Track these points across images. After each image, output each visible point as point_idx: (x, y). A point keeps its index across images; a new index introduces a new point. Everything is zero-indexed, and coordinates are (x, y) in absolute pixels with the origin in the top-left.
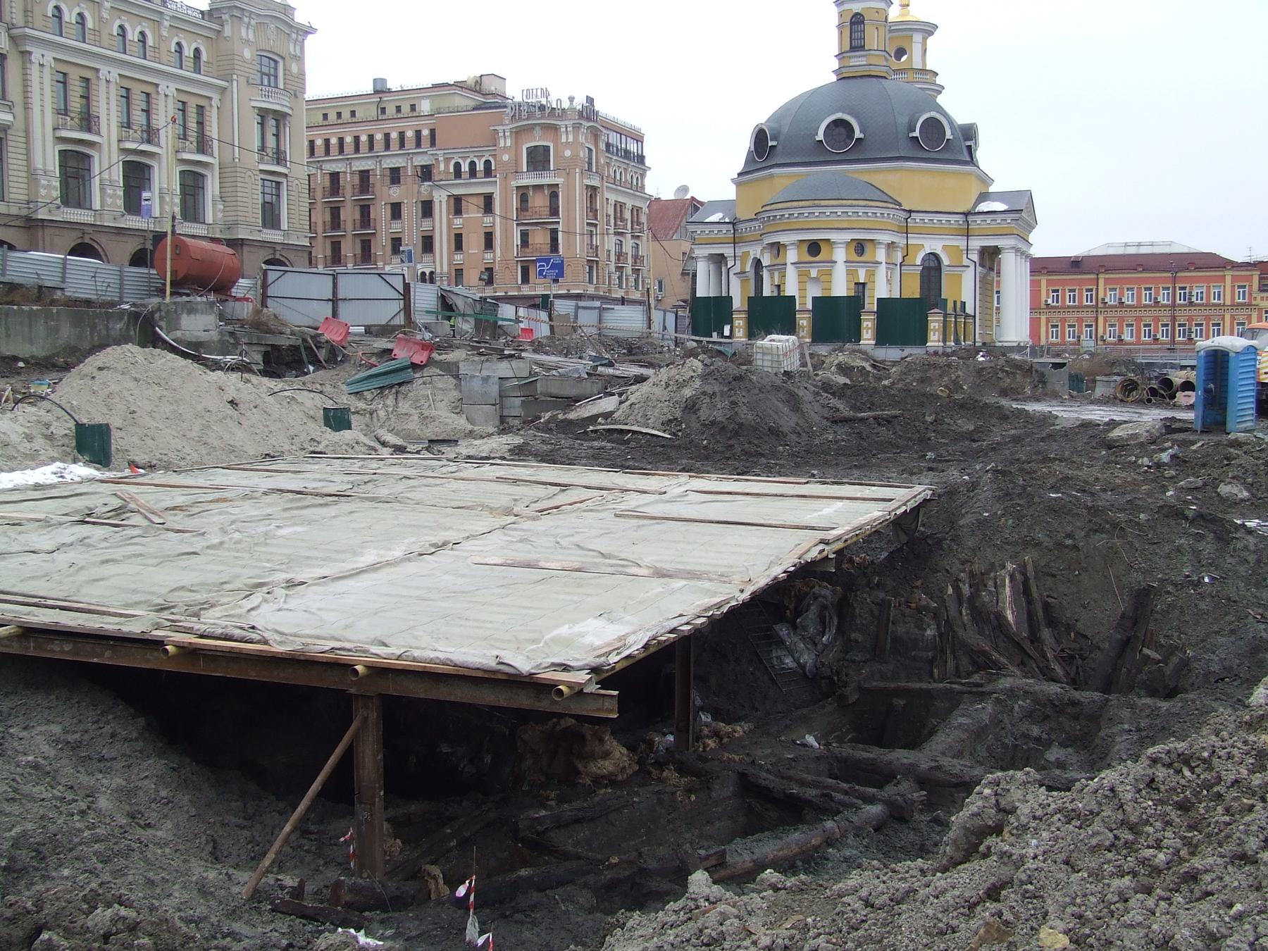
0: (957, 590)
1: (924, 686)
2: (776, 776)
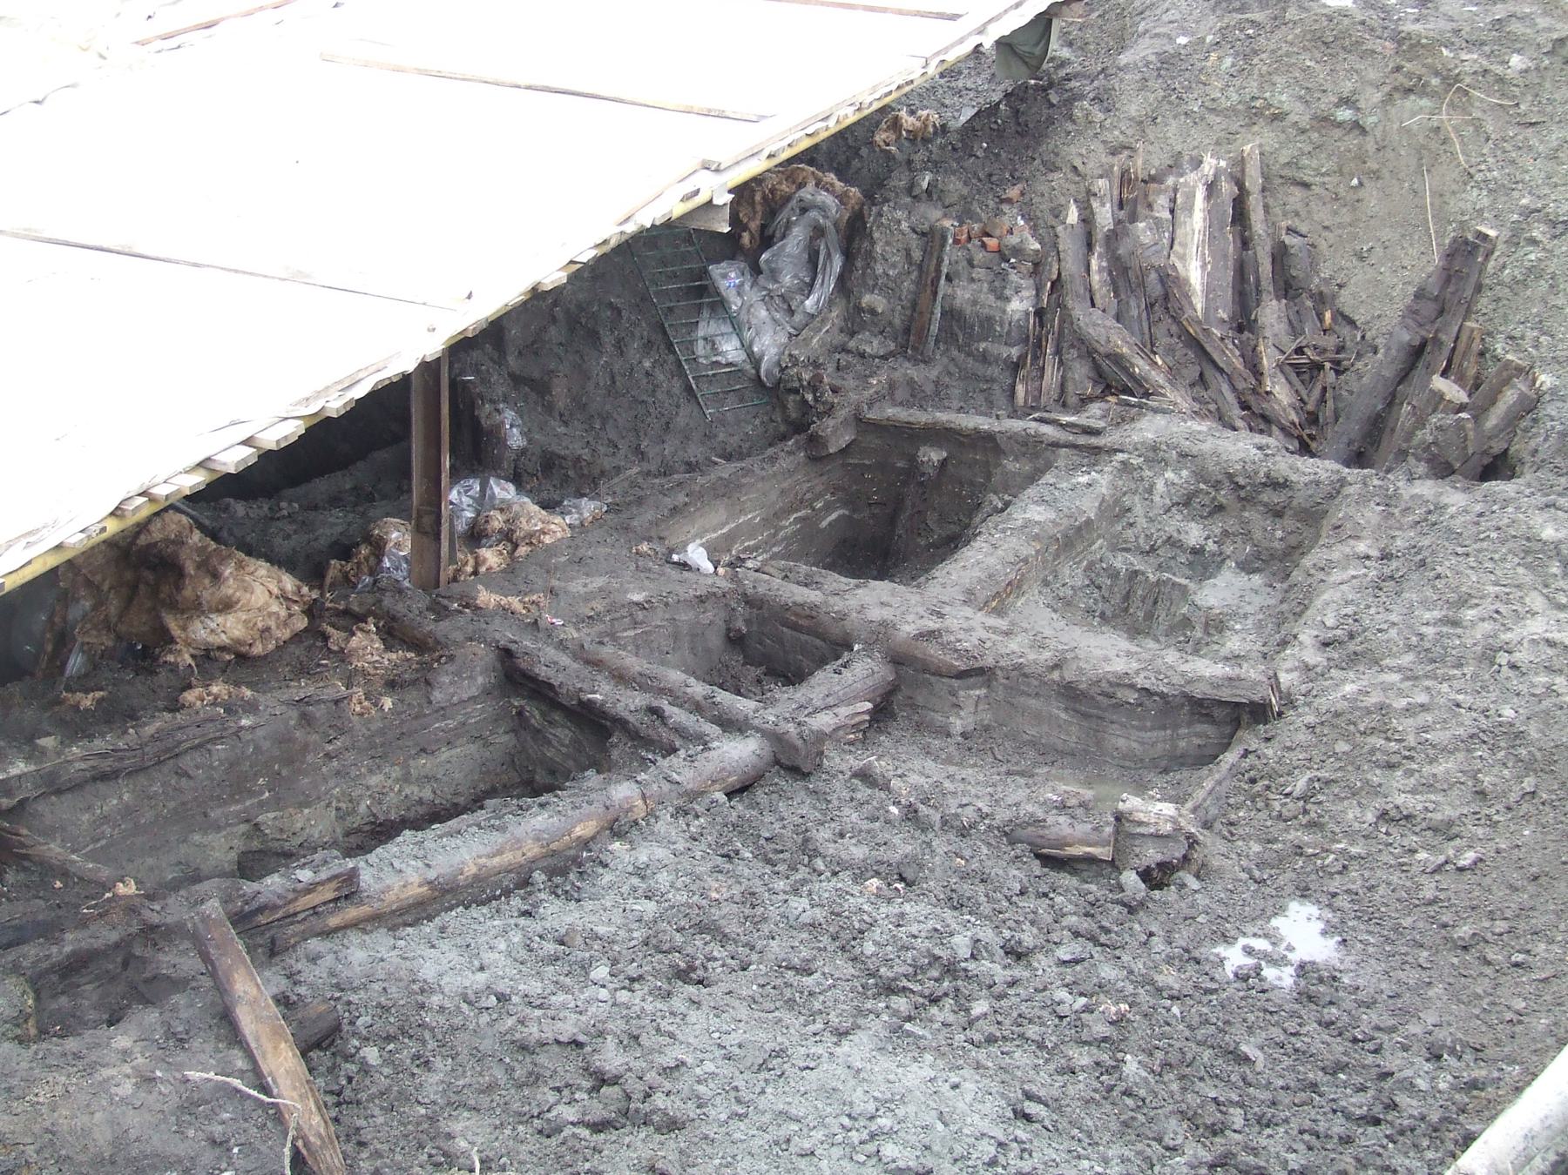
0: (1087, 220)
1: (984, 423)
2: (575, 657)
